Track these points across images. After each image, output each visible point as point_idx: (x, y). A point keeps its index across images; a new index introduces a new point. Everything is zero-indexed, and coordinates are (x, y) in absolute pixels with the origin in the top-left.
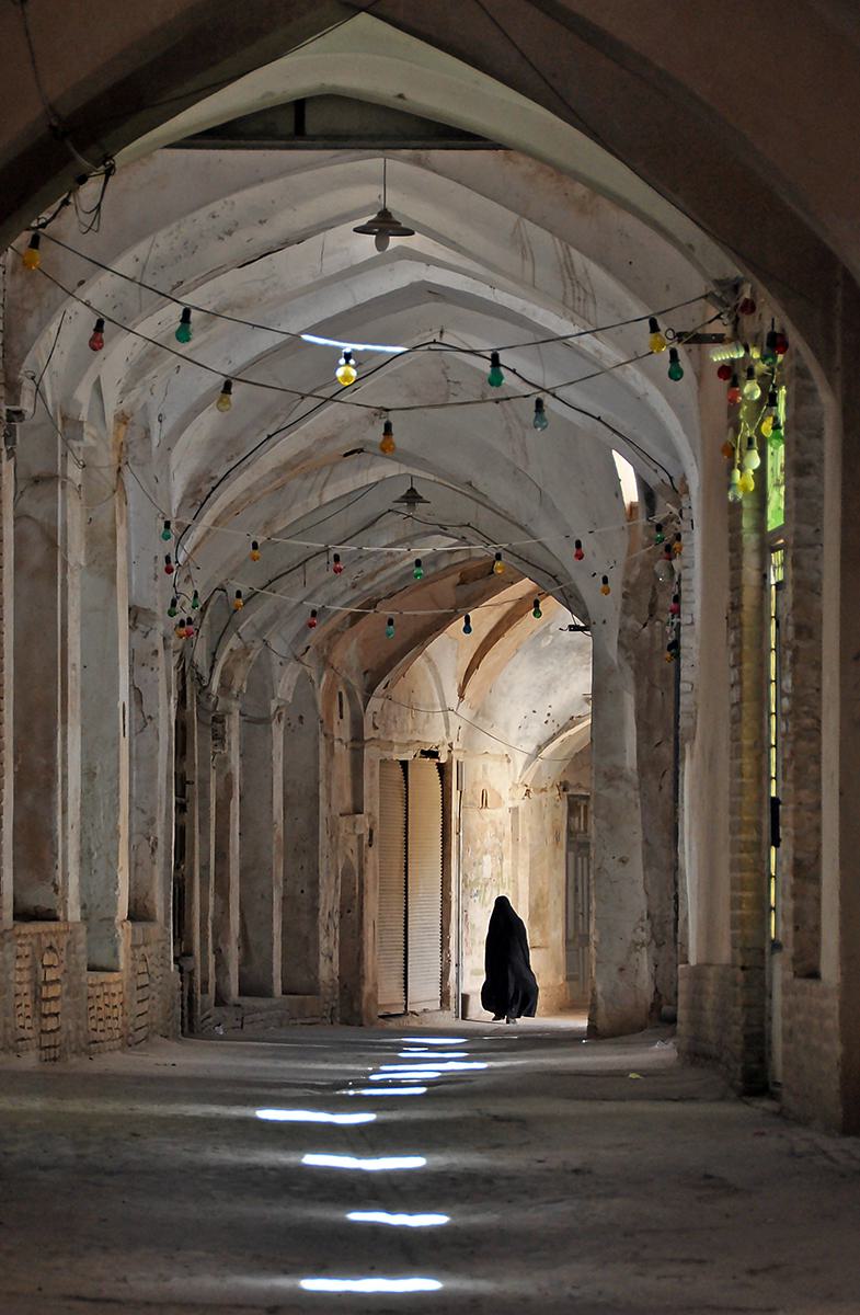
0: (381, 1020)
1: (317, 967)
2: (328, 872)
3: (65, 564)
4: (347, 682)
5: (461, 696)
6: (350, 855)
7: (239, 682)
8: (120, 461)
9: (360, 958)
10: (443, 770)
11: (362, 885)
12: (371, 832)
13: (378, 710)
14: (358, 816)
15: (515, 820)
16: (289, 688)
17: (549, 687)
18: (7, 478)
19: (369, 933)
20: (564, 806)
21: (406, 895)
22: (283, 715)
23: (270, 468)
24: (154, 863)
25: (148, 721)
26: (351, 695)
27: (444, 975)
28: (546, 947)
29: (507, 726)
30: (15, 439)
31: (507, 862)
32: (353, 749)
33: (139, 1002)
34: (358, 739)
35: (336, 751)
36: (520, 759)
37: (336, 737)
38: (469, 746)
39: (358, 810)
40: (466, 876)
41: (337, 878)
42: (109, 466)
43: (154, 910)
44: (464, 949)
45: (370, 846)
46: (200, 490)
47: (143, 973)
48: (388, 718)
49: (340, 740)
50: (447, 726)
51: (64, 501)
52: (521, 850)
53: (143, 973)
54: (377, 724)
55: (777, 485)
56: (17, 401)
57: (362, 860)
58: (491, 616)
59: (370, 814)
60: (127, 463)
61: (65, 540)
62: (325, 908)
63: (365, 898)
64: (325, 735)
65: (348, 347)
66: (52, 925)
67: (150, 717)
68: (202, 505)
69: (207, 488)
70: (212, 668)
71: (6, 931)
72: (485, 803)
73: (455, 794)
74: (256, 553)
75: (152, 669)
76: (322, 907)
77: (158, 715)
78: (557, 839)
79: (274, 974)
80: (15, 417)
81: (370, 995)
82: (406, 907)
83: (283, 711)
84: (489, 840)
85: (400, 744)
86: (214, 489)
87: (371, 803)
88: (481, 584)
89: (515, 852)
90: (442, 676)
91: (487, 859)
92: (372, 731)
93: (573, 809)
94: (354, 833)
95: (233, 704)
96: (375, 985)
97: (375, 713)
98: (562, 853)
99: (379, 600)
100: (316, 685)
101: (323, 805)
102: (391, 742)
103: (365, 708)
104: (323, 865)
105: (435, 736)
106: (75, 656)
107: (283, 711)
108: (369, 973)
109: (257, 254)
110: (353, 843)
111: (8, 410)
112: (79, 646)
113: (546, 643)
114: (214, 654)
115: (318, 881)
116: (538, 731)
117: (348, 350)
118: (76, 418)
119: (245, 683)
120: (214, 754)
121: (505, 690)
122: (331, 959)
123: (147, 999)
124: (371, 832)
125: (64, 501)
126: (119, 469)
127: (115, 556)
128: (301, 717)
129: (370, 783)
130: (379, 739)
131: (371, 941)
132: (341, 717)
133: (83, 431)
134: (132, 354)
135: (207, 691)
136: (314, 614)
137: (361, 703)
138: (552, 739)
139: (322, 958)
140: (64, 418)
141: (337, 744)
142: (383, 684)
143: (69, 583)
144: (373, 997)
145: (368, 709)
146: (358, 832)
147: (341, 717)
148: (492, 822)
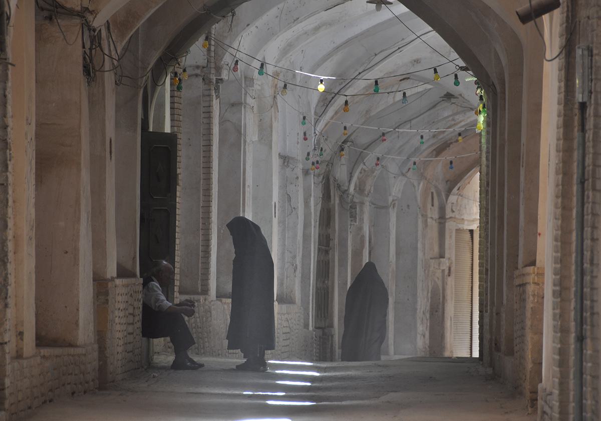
3: (245, 142)
4: (436, 187)
6: (437, 280)
7: (369, 186)
8: (275, 93)
9: (442, 337)
11: (444, 297)
12: (450, 270)
13: (454, 201)
14: (442, 259)
16: (399, 190)
18: (216, 107)
19: (448, 324)
21: (472, 303)
22: (396, 205)
23: (362, 87)
24: (295, 276)
25: (294, 210)
26: (439, 195)
30: (219, 91)
32: (440, 223)
33: (284, 340)
35: (429, 224)
37: (429, 216)
39: (442, 256)
41: (428, 292)
42: (270, 96)
43: (295, 299)
45: (449, 275)
46: (327, 98)
47: (287, 327)
48: (461, 206)
49: (432, 218)
51: (245, 114)
53: (287, 327)
54: (454, 210)
56: (220, 76)
57: (444, 284)
59: (449, 259)
60: (278, 94)
61: (245, 131)
62: (420, 308)
63: (446, 304)
64: (422, 215)
65: (322, 78)
67: (294, 208)
68: (327, 106)
69: (330, 97)
70: (350, 181)
71: (212, 301)
74: (346, 132)
75: (296, 185)
76: (419, 307)
77: (298, 207)
80: (220, 81)
82: (472, 310)
83: (396, 202)
85: (468, 221)
86: (333, 98)
87: (450, 252)
92: (451, 213)
94: (440, 269)
95: (366, 198)
97: (453, 203)
99: (451, 143)
100: (416, 188)
102: (463, 219)
103: (447, 200)
106: (249, 181)
107: (396, 202)
108: (448, 346)
109: (332, 5)
110: (439, 274)
111: (216, 78)
112: (251, 178)
114: (351, 173)
115: (416, 294)
117: (322, 79)
118: (251, 77)
119: (372, 187)
120: (351, 225)
122: (424, 336)
123: (289, 339)
124: (450, 270)
125: (245, 114)
126: (275, 97)
127: (271, 135)
128: (408, 206)
129: (450, 242)
130: (455, 218)
132: (433, 205)
133: (254, 83)
134: (280, 45)
135: (347, 192)
136: (378, 159)
137: (444, 198)
139: (419, 336)
140: (245, 78)
141: (429, 220)
142: (456, 188)
143: (247, 149)
145: (448, 202)
146: (442, 268)
147: (433, 205)
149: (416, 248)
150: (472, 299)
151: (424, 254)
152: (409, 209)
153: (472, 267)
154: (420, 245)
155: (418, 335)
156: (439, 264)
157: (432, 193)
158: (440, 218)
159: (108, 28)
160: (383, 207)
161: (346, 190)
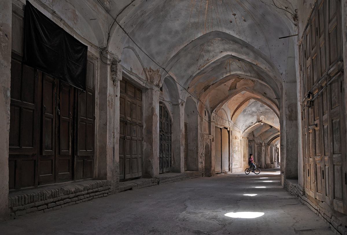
0: (216, 174)
1: (198, 165)
2: (201, 145)
5: (231, 119)
10: (229, 132)
11: (211, 149)
12: (213, 139)
15: (241, 142)
17: (246, 121)
20: (248, 141)
27: (229, 166)
28: (246, 161)
29: (239, 127)
31: (240, 148)
32: (209, 123)
34: (210, 122)
36: (242, 132)
38: (233, 129)
39: (210, 134)
40: (233, 150)
41: (203, 146)
44: (233, 161)
50: (229, 124)
52: (242, 146)
55: (314, 5)
58: (237, 105)
59: (213, 136)
62: (200, 152)
66: (179, 174)
72: (236, 138)
73: (231, 136)
76: (199, 152)
78: (247, 145)
79: (181, 167)
81: (213, 170)
84: (237, 144)
88: (234, 91)
89: (241, 147)
90: (227, 114)
91: (236, 147)
93: (249, 142)
96: (214, 168)
98: (248, 147)
101: (199, 131)
104: (199, 143)
105: (227, 125)
113: (245, 113)
114: (109, 34)
115: (198, 147)
116: (244, 128)
121: (239, 121)
122: (202, 163)
124: (213, 139)
128: (194, 111)
131: (213, 160)
137: (210, 113)
138: (246, 129)
142: (215, 110)
144: (214, 170)
147: (206, 115)
148: (237, 142)
149: (197, 128)
150: (222, 150)
151: (201, 131)
152: (194, 113)
153: (221, 140)
154: (199, 127)
155: (199, 163)
156: (209, 137)
157: (205, 111)
158: (209, 121)
159: (14, 59)
160: (176, 105)
161: (105, 48)
